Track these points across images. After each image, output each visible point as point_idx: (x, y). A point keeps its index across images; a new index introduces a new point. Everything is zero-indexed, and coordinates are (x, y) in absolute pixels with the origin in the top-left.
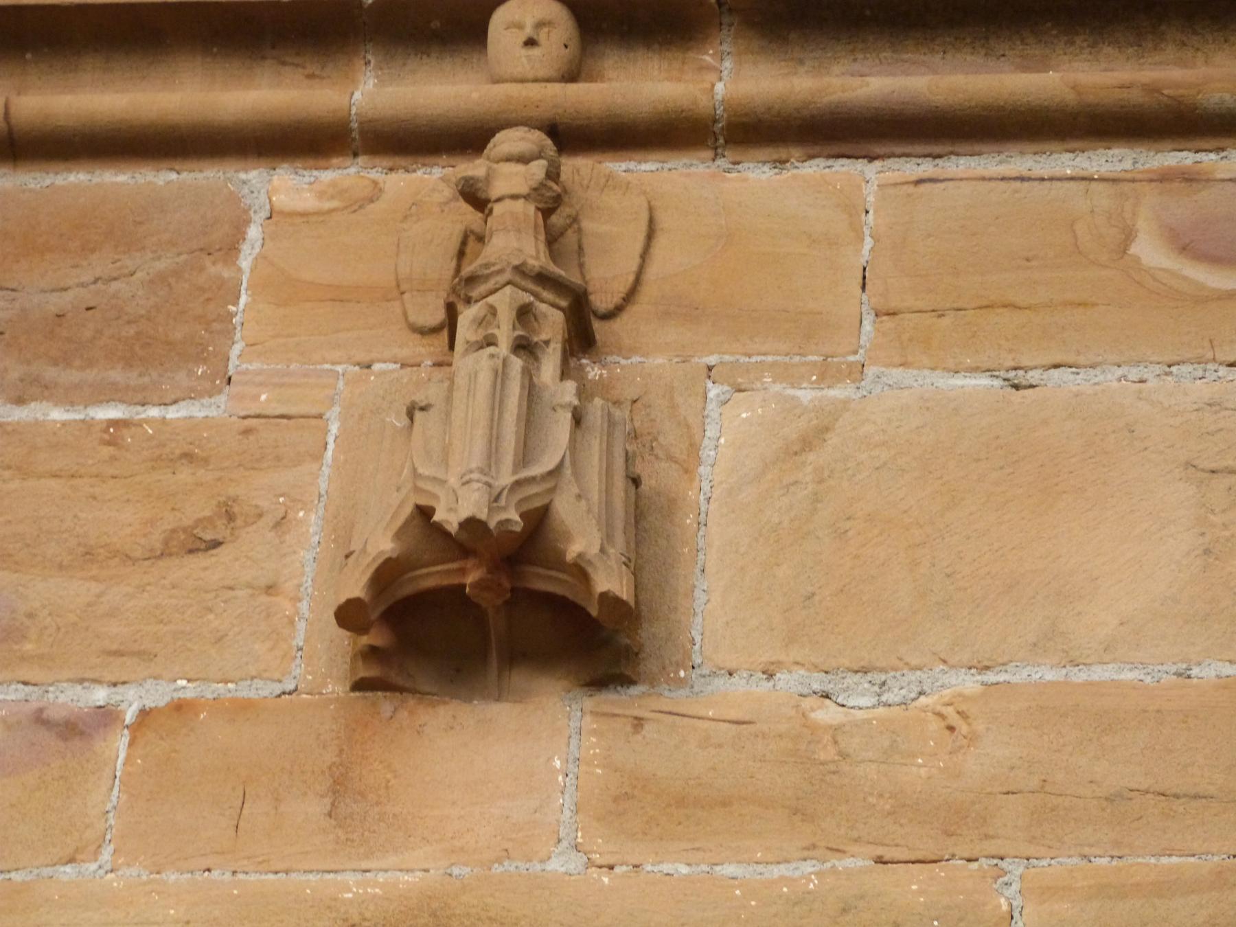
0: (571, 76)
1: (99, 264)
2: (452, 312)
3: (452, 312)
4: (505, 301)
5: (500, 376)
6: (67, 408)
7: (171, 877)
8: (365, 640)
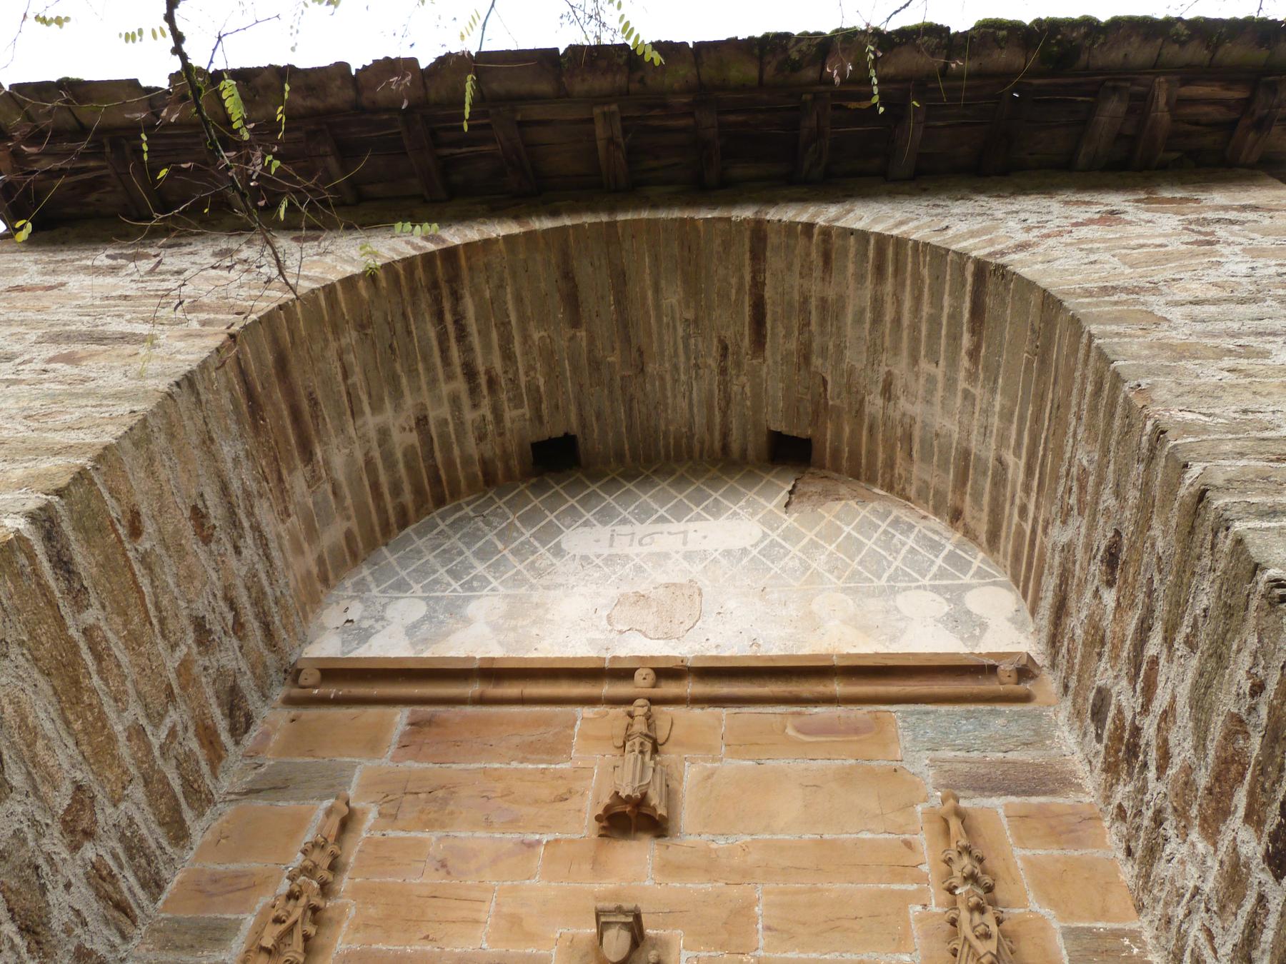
0: (654, 687)
4: (637, 741)
5: (636, 759)
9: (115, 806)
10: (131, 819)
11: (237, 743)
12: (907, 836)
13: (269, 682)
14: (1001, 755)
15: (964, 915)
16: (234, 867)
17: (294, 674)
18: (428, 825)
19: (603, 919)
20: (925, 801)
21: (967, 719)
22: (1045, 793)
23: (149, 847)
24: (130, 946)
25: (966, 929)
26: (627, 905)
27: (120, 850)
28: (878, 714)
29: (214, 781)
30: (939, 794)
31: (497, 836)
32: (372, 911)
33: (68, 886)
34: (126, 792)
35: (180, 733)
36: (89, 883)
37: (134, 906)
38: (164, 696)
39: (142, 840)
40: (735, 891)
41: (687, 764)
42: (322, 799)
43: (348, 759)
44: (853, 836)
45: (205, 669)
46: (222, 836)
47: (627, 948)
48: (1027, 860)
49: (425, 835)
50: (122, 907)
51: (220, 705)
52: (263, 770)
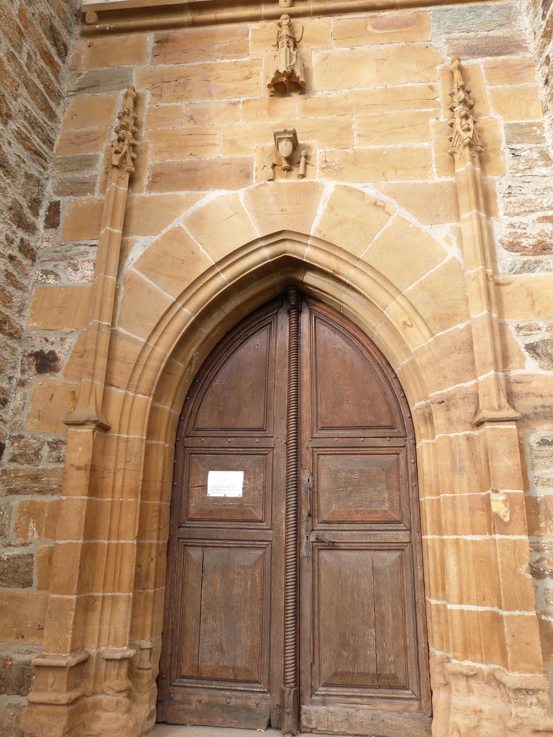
0: (291, 6)
1: (230, 39)
2: (278, 42)
3: (278, 42)
4: (285, 40)
5: (286, 51)
6: (480, 682)
7: (249, 123)
8: (271, 90)
9: (16, 100)
10: (26, 107)
11: (64, 62)
12: (431, 84)
13: (69, 23)
14: (486, 33)
15: (458, 121)
16: (84, 130)
17: (81, 16)
18: (179, 98)
19: (278, 137)
20: (442, 63)
21: (470, 12)
22: (507, 54)
23: (40, 123)
24: (48, 172)
25: (457, 127)
26: (290, 129)
27: (26, 124)
28: (419, 13)
29: (59, 85)
30: (450, 59)
31: (216, 101)
32: (161, 145)
33: (9, 143)
34: (18, 92)
35: (33, 56)
36: (19, 142)
37: (43, 153)
38: (17, 33)
39: (35, 119)
40: (342, 119)
41: (313, 52)
42: (120, 89)
43: (127, 66)
44: (402, 85)
45: (33, 15)
46: (73, 115)
47: (291, 150)
48: (492, 92)
49: (179, 104)
50: (37, 153)
51: (48, 38)
52: (82, 76)
